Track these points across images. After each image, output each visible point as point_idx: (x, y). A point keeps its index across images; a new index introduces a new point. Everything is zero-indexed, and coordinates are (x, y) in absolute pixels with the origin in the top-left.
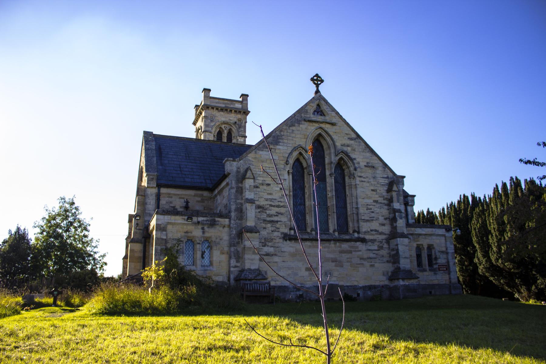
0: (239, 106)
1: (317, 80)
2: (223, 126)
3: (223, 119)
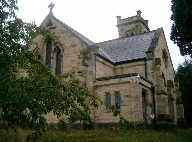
0: (136, 19)
1: (52, 6)
2: (128, 33)
3: (128, 29)
